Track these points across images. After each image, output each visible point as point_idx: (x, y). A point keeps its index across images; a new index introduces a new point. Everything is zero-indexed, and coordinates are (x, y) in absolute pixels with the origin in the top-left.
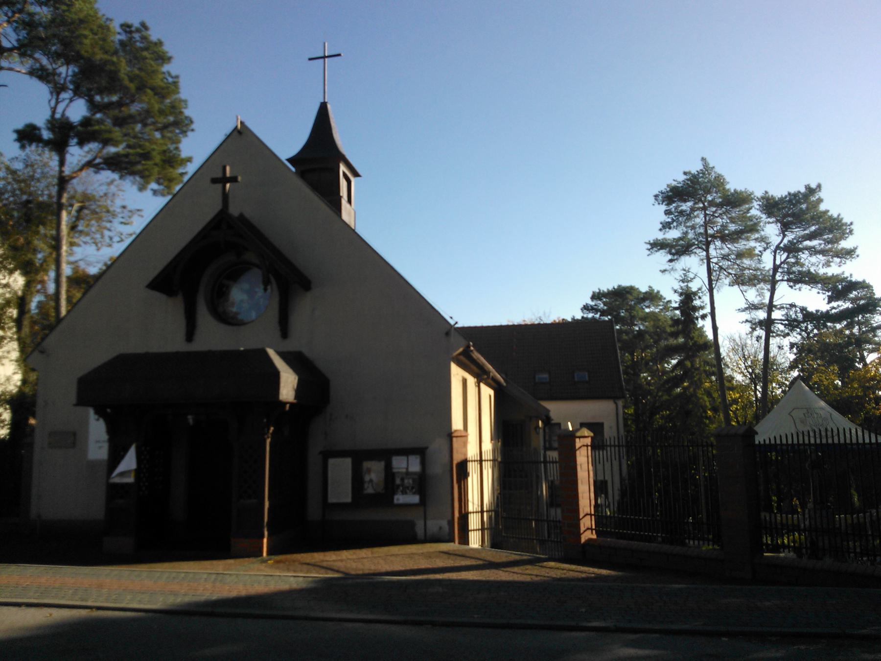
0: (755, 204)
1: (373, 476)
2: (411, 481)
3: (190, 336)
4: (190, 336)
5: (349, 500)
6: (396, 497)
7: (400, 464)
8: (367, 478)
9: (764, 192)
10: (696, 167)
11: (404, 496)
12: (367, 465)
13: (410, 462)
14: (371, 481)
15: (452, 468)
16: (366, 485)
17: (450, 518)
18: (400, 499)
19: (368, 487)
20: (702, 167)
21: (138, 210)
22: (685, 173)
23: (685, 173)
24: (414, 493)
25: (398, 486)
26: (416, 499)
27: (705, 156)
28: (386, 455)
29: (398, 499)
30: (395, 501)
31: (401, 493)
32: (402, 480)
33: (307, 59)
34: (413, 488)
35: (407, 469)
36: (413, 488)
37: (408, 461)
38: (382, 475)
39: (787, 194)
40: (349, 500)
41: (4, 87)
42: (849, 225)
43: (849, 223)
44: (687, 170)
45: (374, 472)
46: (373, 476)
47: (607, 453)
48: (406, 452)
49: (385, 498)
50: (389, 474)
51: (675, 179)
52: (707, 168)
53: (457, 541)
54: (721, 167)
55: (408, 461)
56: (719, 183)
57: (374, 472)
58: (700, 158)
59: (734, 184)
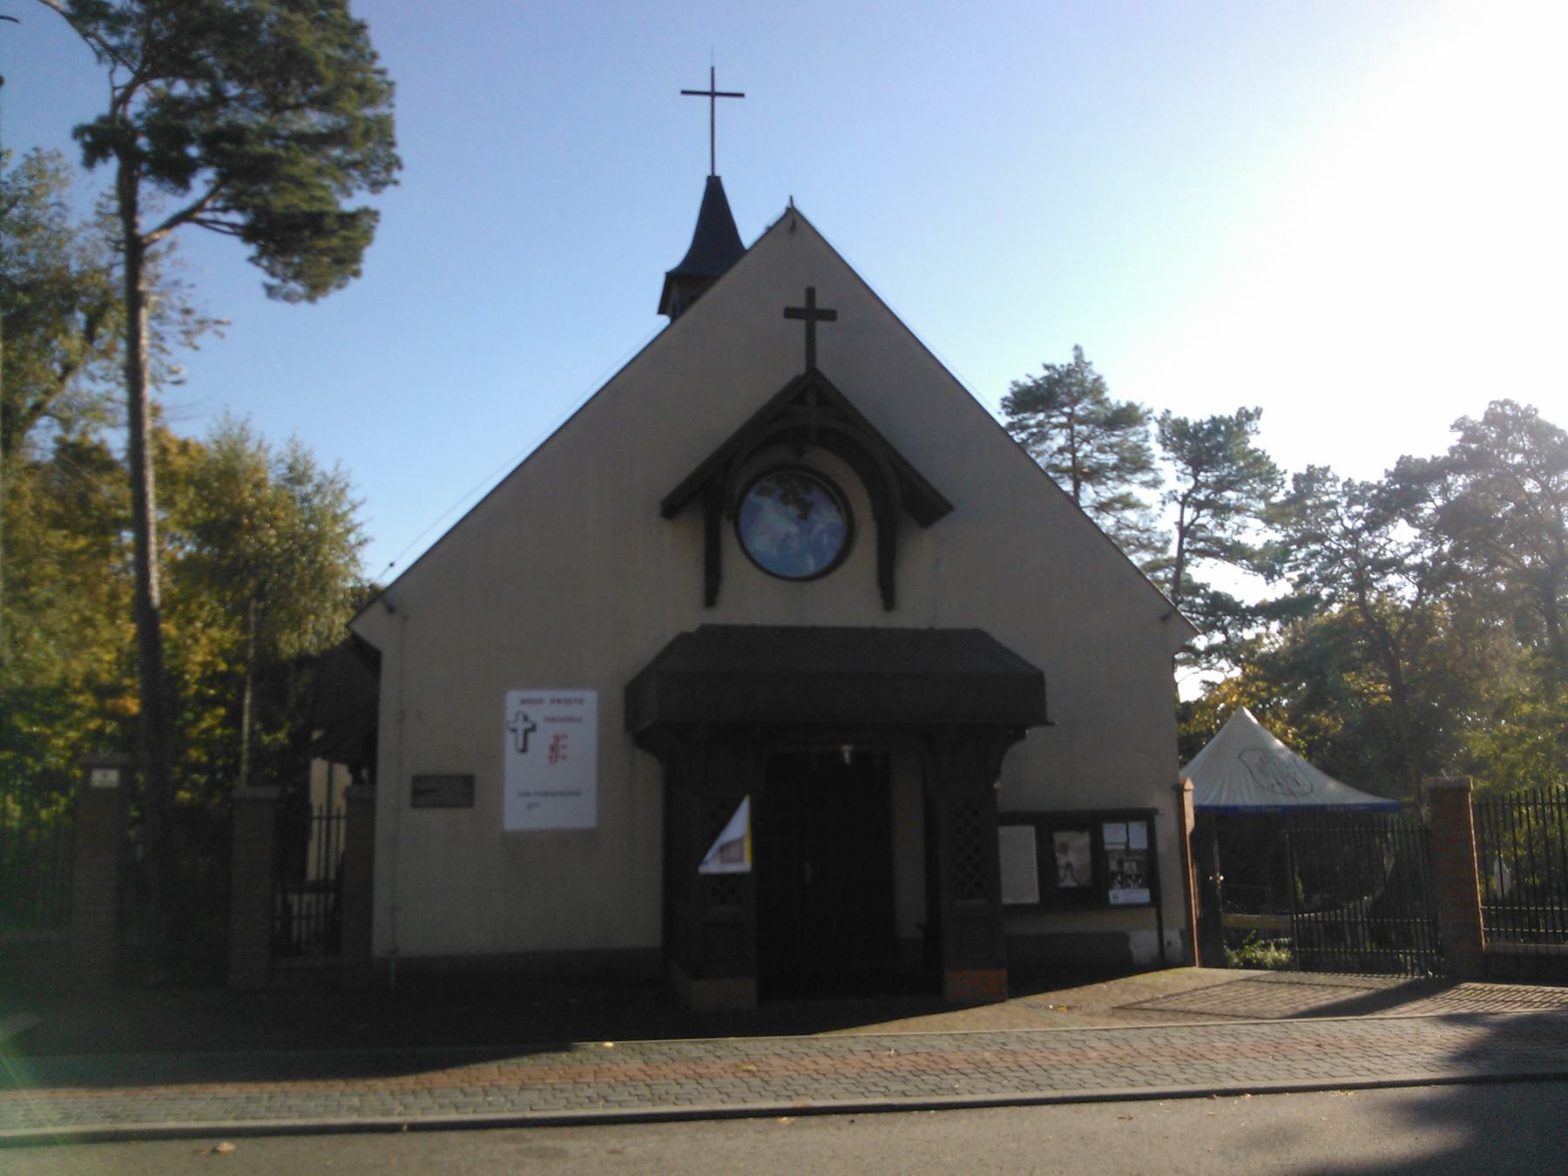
0: (1153, 428)
1: (1072, 857)
2: (1134, 865)
3: (711, 596)
4: (711, 596)
5: (1033, 898)
6: (1111, 893)
7: (1114, 835)
8: (1062, 860)
9: (1164, 411)
10: (1064, 359)
11: (1127, 891)
12: (1060, 837)
13: (1130, 831)
14: (1069, 865)
15: (1183, 842)
16: (1062, 873)
17: (1183, 926)
18: (1118, 895)
19: (1065, 876)
20: (1072, 361)
21: (218, 322)
22: (1047, 367)
23: (1047, 367)
24: (1141, 886)
25: (1114, 875)
26: (1143, 896)
27: (1080, 344)
28: (1091, 822)
29: (1116, 897)
30: (1112, 901)
31: (1118, 886)
32: (1120, 863)
33: (679, 92)
34: (1138, 877)
35: (1127, 844)
36: (1138, 877)
37: (1127, 828)
38: (1086, 858)
39: (1209, 418)
40: (1033, 898)
41: (12, 22)
42: (1281, 474)
43: (1282, 471)
44: (1048, 362)
45: (1074, 852)
46: (1072, 857)
47: (337, 846)
48: (1125, 816)
49: (1092, 895)
50: (1098, 850)
51: (1030, 374)
52: (1080, 362)
53: (1197, 965)
54: (1101, 365)
55: (1127, 828)
56: (1096, 390)
57: (1074, 852)
58: (1072, 346)
59: (1117, 395)
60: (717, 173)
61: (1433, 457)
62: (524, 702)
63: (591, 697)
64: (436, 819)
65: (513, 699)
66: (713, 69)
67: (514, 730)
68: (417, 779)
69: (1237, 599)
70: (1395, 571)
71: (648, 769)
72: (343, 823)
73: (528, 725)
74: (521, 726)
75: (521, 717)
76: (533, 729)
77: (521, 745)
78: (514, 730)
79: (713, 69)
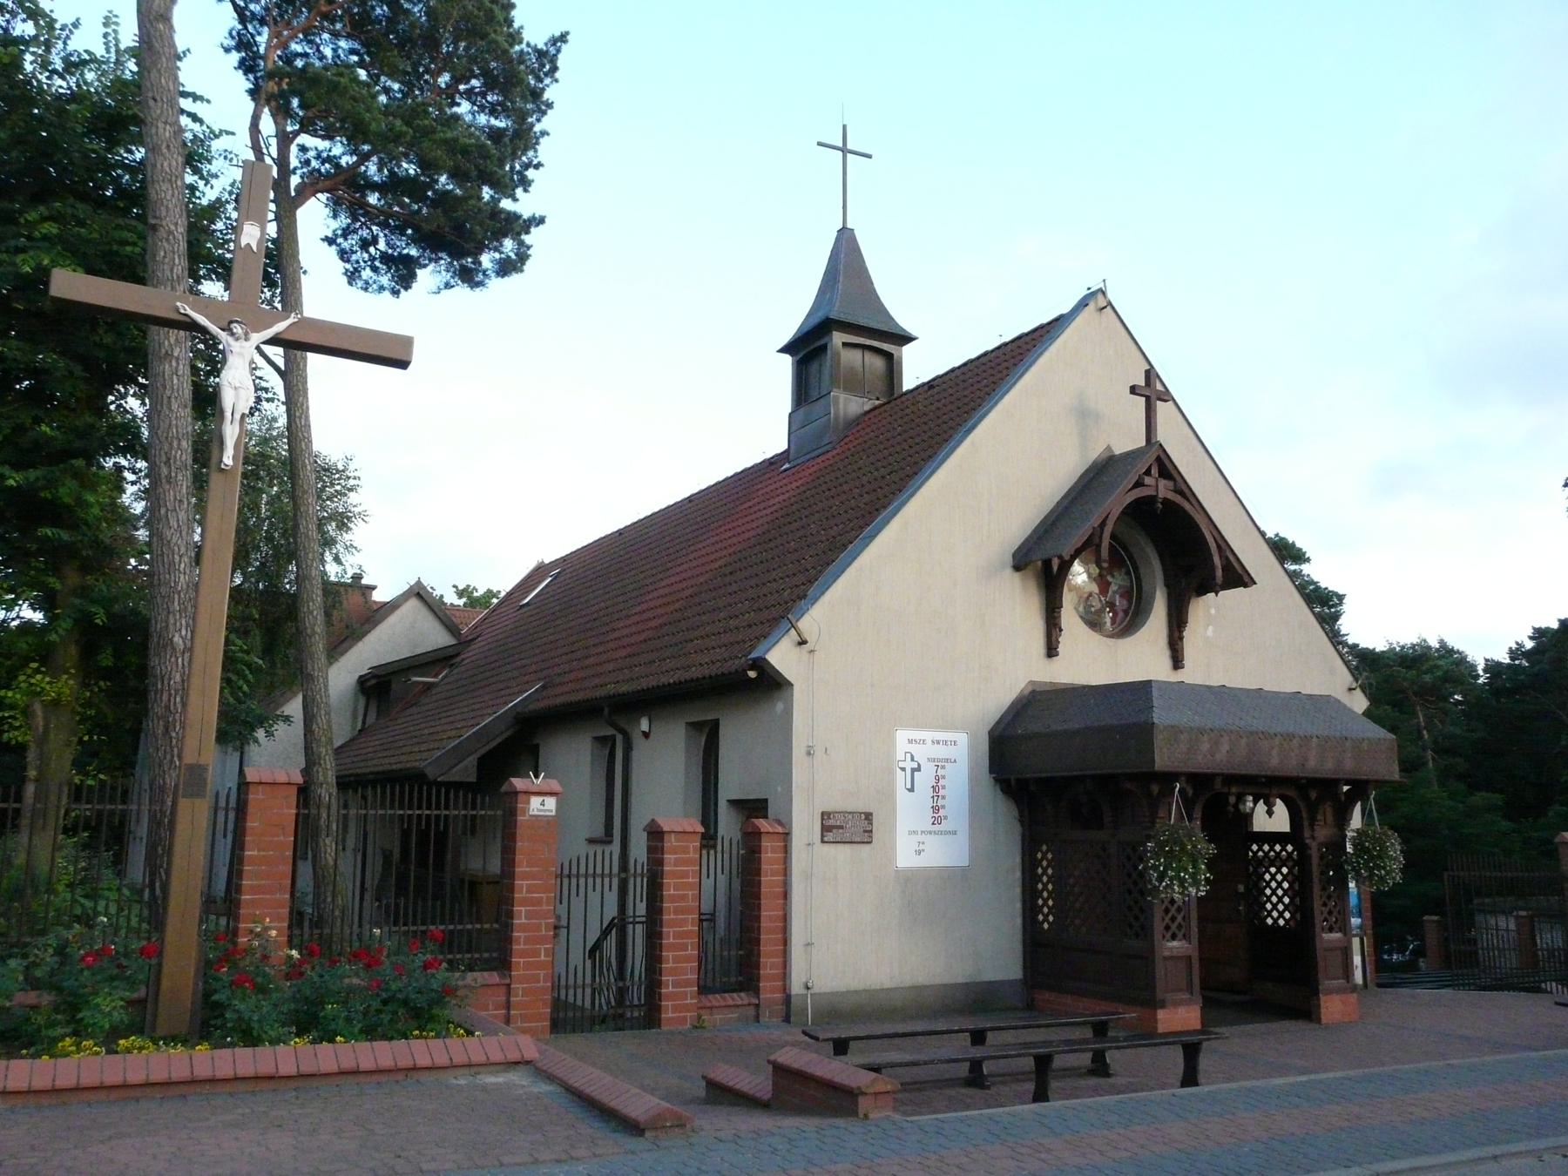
3: (1051, 650)
60: (849, 226)
61: (1559, 620)
62: (910, 741)
63: (962, 738)
64: (841, 854)
65: (902, 736)
66: (844, 127)
67: (903, 769)
68: (825, 815)
69: (1371, 648)
70: (1455, 653)
71: (1004, 820)
72: (639, 928)
73: (915, 765)
74: (909, 765)
75: (908, 756)
76: (918, 769)
77: (909, 786)
78: (903, 769)
79: (844, 127)
